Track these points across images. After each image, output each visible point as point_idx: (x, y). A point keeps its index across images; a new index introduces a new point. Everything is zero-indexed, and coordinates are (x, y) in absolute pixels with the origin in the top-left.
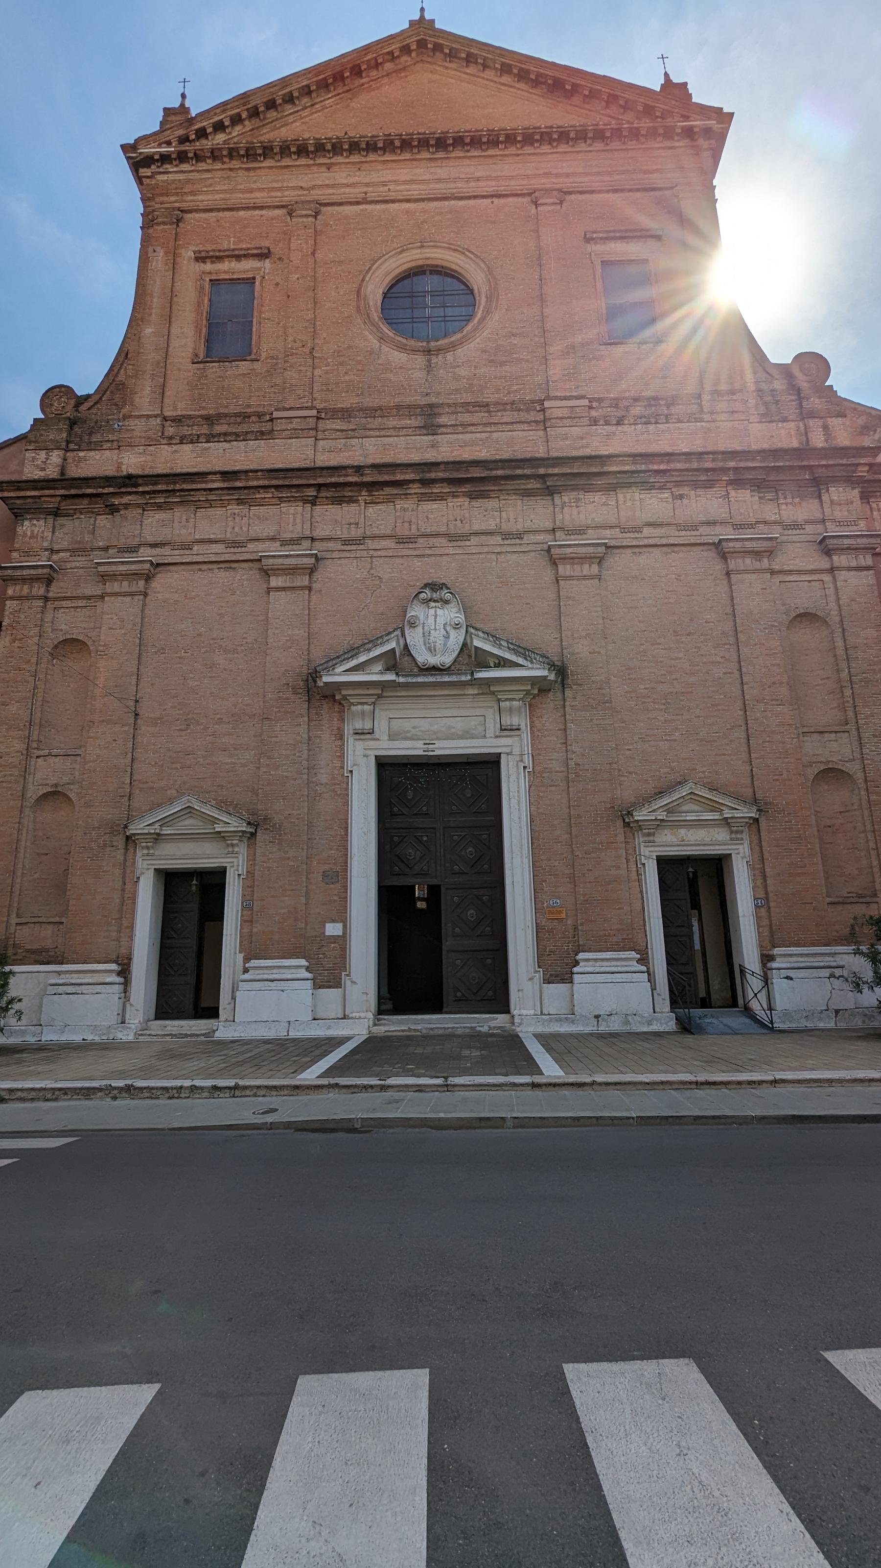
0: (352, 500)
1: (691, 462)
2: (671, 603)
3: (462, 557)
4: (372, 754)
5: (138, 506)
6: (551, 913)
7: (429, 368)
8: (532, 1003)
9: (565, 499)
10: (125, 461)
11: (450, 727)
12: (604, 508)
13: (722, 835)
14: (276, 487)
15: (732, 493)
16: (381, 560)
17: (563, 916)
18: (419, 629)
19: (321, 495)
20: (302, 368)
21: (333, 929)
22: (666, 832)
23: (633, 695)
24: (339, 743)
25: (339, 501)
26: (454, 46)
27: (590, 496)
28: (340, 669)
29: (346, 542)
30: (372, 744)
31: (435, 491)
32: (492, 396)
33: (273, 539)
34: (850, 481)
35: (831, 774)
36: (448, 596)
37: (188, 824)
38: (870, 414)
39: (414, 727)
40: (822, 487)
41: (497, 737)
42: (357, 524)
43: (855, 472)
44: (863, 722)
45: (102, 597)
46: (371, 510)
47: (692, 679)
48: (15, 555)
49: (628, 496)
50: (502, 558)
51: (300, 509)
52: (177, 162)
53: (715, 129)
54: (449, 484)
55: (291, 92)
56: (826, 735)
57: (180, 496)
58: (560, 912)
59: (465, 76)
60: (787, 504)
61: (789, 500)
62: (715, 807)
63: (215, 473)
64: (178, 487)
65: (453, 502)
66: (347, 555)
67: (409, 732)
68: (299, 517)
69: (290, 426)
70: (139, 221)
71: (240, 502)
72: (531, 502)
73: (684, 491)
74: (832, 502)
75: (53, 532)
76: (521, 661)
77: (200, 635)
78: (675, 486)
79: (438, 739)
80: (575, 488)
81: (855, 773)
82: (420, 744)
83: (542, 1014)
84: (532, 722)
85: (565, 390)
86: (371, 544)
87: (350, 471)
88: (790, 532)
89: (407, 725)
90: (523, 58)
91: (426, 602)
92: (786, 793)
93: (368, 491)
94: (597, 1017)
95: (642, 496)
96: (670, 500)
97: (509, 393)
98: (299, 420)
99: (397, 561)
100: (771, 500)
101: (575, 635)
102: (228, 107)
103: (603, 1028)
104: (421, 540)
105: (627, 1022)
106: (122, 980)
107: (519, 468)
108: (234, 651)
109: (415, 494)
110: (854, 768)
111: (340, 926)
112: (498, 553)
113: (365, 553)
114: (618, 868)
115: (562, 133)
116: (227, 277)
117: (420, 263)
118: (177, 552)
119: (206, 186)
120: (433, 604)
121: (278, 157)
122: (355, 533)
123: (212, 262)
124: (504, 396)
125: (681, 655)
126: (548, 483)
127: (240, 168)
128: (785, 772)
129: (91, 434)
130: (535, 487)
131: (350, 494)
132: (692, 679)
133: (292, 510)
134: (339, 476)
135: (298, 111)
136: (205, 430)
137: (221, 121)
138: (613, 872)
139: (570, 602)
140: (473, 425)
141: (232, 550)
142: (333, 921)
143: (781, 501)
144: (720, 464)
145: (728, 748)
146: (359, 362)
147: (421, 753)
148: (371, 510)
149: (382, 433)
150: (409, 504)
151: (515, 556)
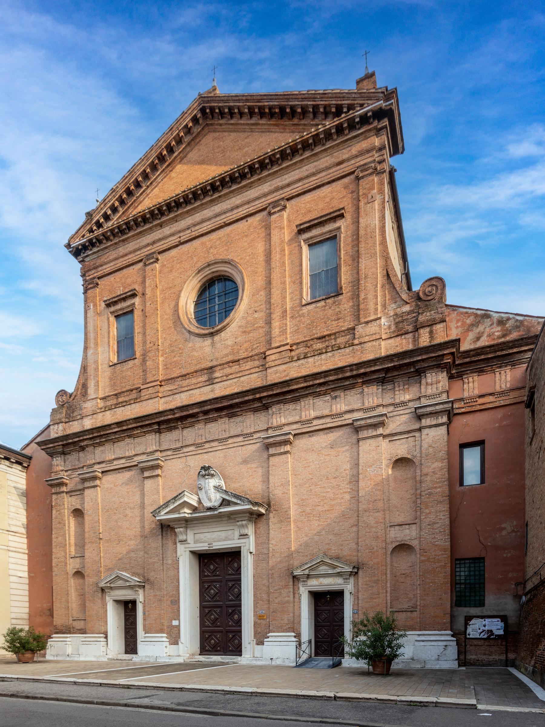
0: (176, 428)
1: (338, 374)
2: (326, 462)
3: (225, 450)
4: (188, 550)
5: (91, 445)
6: (260, 616)
7: (213, 344)
8: (252, 653)
9: (274, 410)
10: (86, 424)
11: (219, 536)
12: (294, 412)
13: (340, 580)
14: (142, 427)
15: (366, 390)
16: (190, 457)
17: (265, 618)
18: (203, 490)
19: (161, 428)
20: (154, 358)
21: (175, 623)
22: (313, 580)
23: (304, 513)
24: (175, 546)
25: (170, 429)
26: (220, 105)
27: (287, 406)
28: (163, 513)
29: (175, 450)
30: (187, 546)
31: (211, 416)
32: (243, 354)
33: (144, 453)
34: (439, 367)
35: (403, 548)
36: (212, 472)
37: (120, 583)
38: (476, 314)
39: (205, 537)
40: (422, 375)
41: (239, 539)
42: (179, 440)
43: (442, 360)
44: (424, 517)
45: (420, 430)
46: (185, 432)
47: (334, 503)
48: (53, 474)
49: (307, 402)
50: (244, 448)
51: (154, 436)
52: (91, 247)
53: (383, 108)
54: (216, 411)
55: (136, 179)
56: (403, 526)
57: (105, 438)
58: (264, 616)
59: (231, 127)
60: (399, 391)
61: (401, 388)
62: (334, 567)
63: (113, 424)
64: (102, 433)
65: (220, 421)
66: (175, 456)
67: (202, 539)
68: (154, 440)
69: (148, 392)
70: (82, 289)
71: (129, 437)
72: (258, 415)
73: (337, 393)
74: (427, 383)
75: (65, 462)
76: (239, 502)
77: (121, 502)
78: (332, 391)
79: (214, 542)
80: (279, 402)
81: (416, 546)
82: (206, 544)
83: (254, 657)
84: (255, 531)
85: (280, 341)
86: (186, 450)
87: (113, 426)
88: (399, 409)
89: (202, 536)
90: (259, 98)
91: (204, 476)
92: (374, 559)
93: (182, 422)
94: (271, 659)
95: (314, 401)
96: (330, 400)
97: (252, 350)
98: (151, 388)
99: (197, 456)
100: (390, 390)
101: (276, 485)
102: (106, 201)
103: (274, 663)
104: (207, 445)
105: (284, 662)
106: (105, 640)
107: (246, 396)
108: (134, 508)
109: (202, 419)
110: (415, 543)
111: (177, 621)
112: (242, 446)
113: (183, 455)
114: (289, 596)
115: (282, 151)
116: (121, 312)
117: (210, 276)
118: (108, 465)
119: (106, 259)
120: (207, 477)
121: (142, 224)
122: (178, 445)
123: (114, 305)
124: (250, 353)
125: (329, 490)
126: (264, 402)
127: (120, 241)
128: (375, 548)
129: (73, 412)
130: (258, 405)
131: (173, 425)
132: (334, 503)
133: (151, 437)
134: (164, 416)
135: (144, 191)
136: (115, 401)
137: (105, 213)
138: (287, 599)
139: (274, 468)
140: (231, 374)
141: (129, 461)
142: (175, 620)
143: (397, 389)
144: (355, 373)
145: (349, 537)
146: (180, 348)
147: (207, 548)
148: (186, 432)
149: (189, 388)
150: (200, 426)
151: (249, 446)
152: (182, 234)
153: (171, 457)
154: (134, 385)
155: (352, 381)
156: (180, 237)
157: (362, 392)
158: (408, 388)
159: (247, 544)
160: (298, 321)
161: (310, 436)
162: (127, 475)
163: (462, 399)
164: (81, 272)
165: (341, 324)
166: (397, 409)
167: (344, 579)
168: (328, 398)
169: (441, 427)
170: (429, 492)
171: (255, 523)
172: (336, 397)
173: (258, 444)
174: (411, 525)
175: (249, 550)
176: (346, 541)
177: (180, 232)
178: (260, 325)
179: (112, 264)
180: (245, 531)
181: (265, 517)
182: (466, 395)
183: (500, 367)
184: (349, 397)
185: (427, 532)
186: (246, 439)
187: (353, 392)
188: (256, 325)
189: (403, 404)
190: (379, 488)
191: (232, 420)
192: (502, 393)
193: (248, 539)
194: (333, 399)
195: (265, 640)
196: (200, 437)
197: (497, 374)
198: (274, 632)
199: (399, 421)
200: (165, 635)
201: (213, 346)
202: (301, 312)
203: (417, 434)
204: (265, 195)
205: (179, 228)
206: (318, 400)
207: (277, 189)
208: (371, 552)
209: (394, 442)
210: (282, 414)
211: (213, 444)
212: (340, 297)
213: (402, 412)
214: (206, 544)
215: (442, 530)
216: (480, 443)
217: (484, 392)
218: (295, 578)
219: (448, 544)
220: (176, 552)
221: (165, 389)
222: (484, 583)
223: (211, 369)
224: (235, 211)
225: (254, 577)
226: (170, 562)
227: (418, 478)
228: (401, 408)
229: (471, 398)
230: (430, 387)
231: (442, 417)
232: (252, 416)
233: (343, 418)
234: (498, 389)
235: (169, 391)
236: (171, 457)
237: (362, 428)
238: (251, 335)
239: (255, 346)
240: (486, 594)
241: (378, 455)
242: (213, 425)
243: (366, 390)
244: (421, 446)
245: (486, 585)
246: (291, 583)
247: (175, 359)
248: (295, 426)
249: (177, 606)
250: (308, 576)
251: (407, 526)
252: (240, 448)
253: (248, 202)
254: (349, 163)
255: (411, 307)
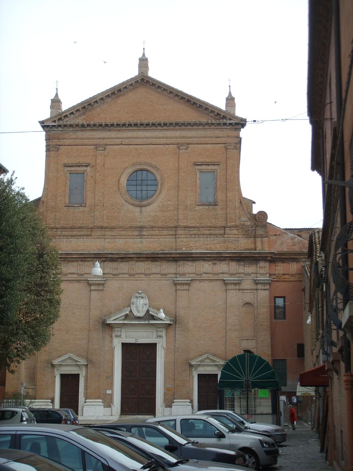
7: (141, 211)
15: (231, 263)
17: (171, 390)
21: (109, 392)
24: (111, 338)
27: (188, 262)
30: (120, 339)
31: (141, 259)
45: (257, 290)
49: (199, 263)
56: (249, 340)
66: (114, 279)
74: (260, 267)
82: (134, 340)
84: (166, 334)
88: (247, 276)
113: (119, 279)
114: (187, 377)
140: (154, 235)
142: (109, 390)
152: (123, 140)
153: (111, 279)
154: (83, 224)
155: (224, 258)
156: (122, 141)
157: (229, 264)
158: (251, 266)
159: (161, 342)
160: (194, 213)
161: (200, 282)
162: (76, 285)
163: (275, 274)
164: (46, 138)
165: (217, 222)
166: (245, 276)
167: (218, 368)
168: (211, 263)
169: (266, 291)
170: (261, 324)
171: (166, 329)
172: (215, 264)
173: (169, 281)
174: (252, 340)
175: (163, 346)
176: (219, 345)
177: (122, 138)
178: (171, 209)
179: (71, 141)
180: (159, 334)
181: (172, 326)
182: (277, 272)
183: (292, 262)
184: (221, 265)
185: (260, 345)
186: (162, 277)
187: (224, 262)
188: (168, 209)
189: (249, 274)
190: (237, 318)
191: (153, 263)
192: (292, 275)
193: (161, 339)
194: (214, 265)
195: (173, 404)
196: (132, 270)
197: (290, 264)
198: (177, 399)
199: (247, 284)
200: (101, 400)
201: (141, 213)
202: (195, 209)
203: (255, 291)
204: (176, 138)
205: (122, 136)
206: (205, 263)
207: (183, 137)
208: (233, 353)
209: (244, 293)
210: (185, 267)
211: (140, 275)
212: (217, 207)
213: (248, 278)
214: (134, 340)
215: (267, 345)
216: (284, 297)
217: (284, 273)
218: (191, 366)
219: (270, 352)
220: (112, 343)
221: (109, 234)
222: (286, 373)
223: (142, 228)
224: (158, 140)
225: (165, 363)
226: (107, 349)
227: (256, 315)
228: (248, 276)
229: (279, 274)
230: (261, 269)
231: (267, 286)
232: (166, 263)
233: (219, 276)
234: (291, 273)
235: (112, 235)
236: (111, 279)
237: (229, 284)
238: (166, 213)
239: (168, 221)
240: (287, 379)
241: (235, 297)
242: (141, 263)
243: (231, 263)
244: (257, 299)
245: (287, 373)
246: (188, 369)
247: (115, 214)
248: (192, 275)
249: (111, 380)
250: (199, 365)
251: (250, 341)
252: (158, 281)
253: (167, 138)
254: (222, 139)
255: (251, 223)
